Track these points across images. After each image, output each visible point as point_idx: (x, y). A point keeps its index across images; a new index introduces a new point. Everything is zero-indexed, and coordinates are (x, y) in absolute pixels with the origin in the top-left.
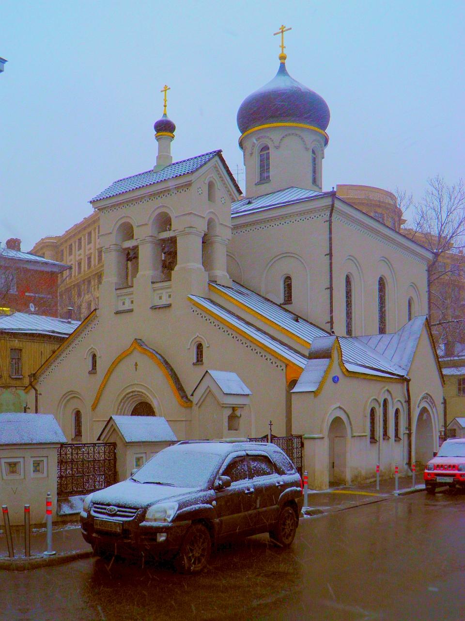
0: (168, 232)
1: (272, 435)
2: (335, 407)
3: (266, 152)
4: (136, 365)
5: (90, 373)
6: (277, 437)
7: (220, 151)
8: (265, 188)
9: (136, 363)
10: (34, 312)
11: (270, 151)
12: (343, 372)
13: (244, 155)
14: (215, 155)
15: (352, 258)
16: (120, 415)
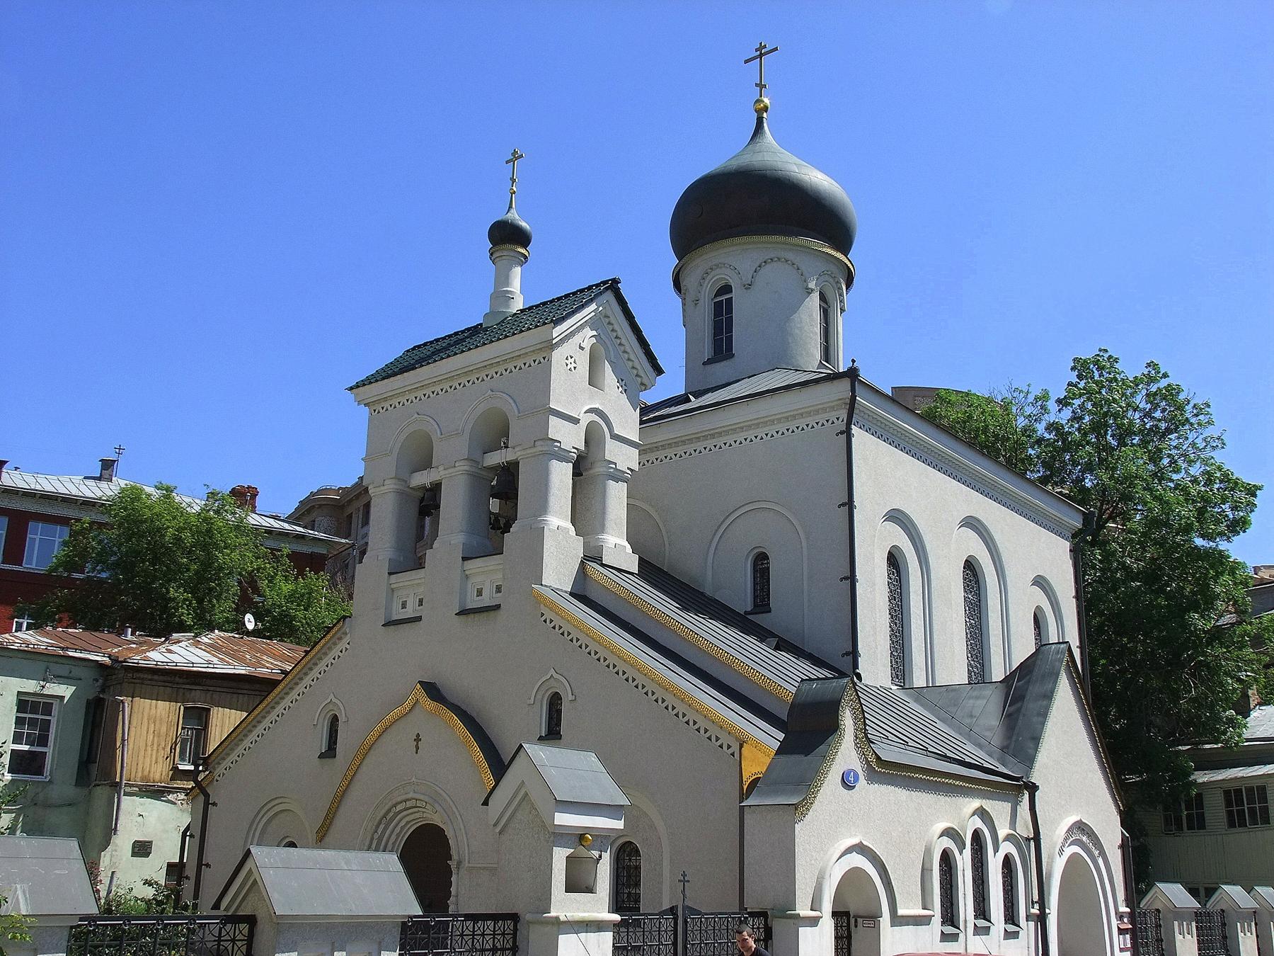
0: (504, 451)
1: (685, 908)
2: (843, 848)
3: (728, 296)
4: (418, 739)
5: (322, 756)
6: (699, 913)
7: (615, 281)
8: (721, 370)
9: (418, 735)
10: (254, 630)
11: (733, 295)
12: (868, 762)
13: (684, 304)
14: (607, 289)
15: (896, 517)
16: (377, 850)
